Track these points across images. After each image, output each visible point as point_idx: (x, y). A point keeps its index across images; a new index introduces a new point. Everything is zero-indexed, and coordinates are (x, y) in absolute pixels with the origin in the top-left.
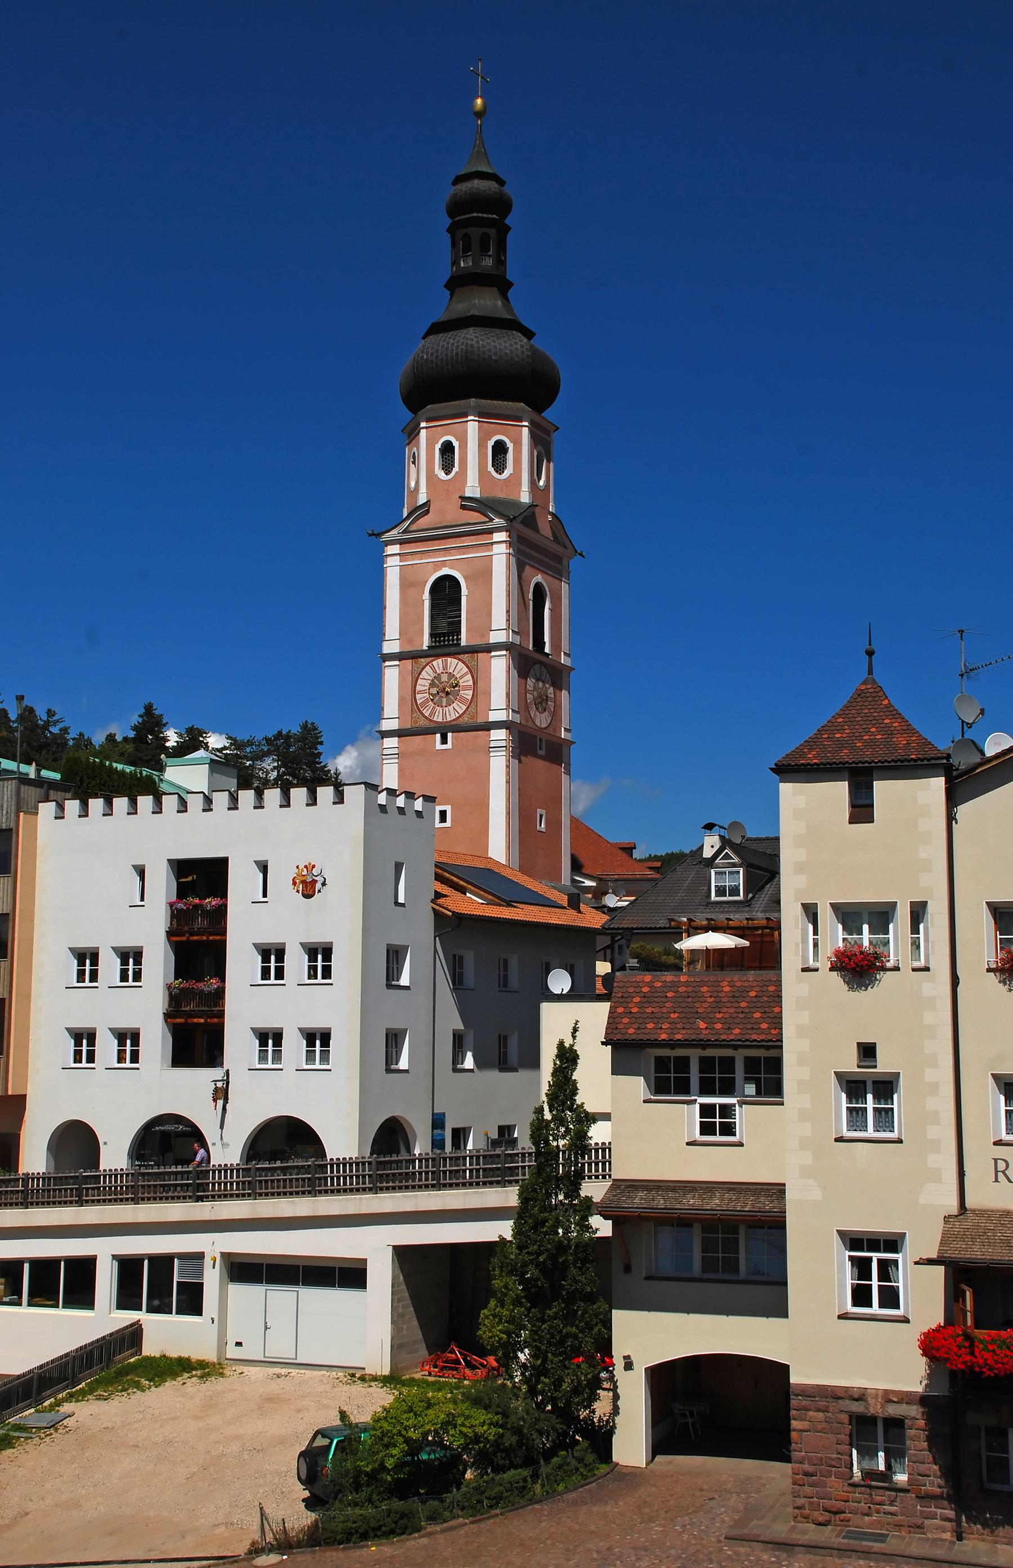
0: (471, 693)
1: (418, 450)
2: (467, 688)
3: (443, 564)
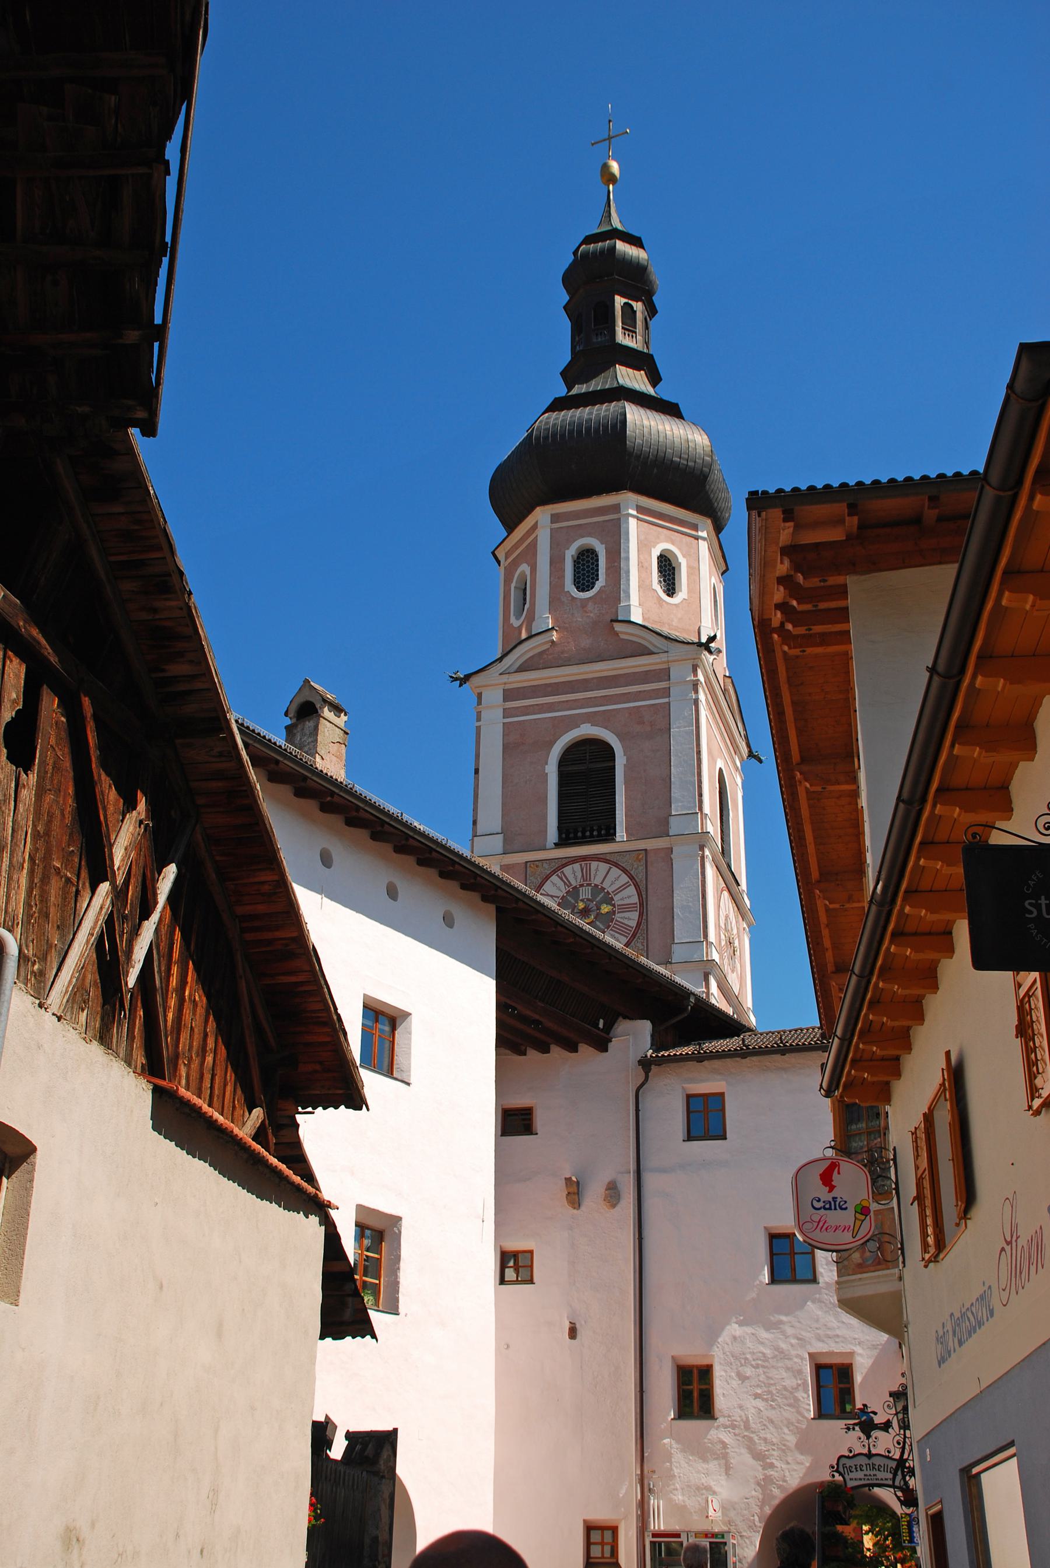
0: (635, 915)
1: (534, 570)
2: (626, 908)
3: (574, 722)
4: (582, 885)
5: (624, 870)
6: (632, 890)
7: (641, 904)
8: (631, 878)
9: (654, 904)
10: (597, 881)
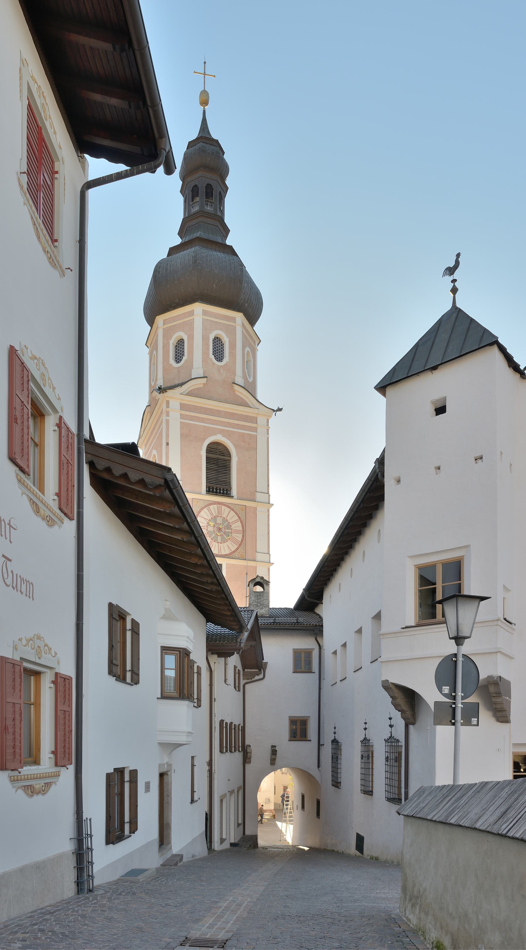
3: (215, 432)
5: (236, 513)
6: (239, 524)
7: (243, 531)
8: (239, 518)
9: (248, 532)
10: (225, 516)
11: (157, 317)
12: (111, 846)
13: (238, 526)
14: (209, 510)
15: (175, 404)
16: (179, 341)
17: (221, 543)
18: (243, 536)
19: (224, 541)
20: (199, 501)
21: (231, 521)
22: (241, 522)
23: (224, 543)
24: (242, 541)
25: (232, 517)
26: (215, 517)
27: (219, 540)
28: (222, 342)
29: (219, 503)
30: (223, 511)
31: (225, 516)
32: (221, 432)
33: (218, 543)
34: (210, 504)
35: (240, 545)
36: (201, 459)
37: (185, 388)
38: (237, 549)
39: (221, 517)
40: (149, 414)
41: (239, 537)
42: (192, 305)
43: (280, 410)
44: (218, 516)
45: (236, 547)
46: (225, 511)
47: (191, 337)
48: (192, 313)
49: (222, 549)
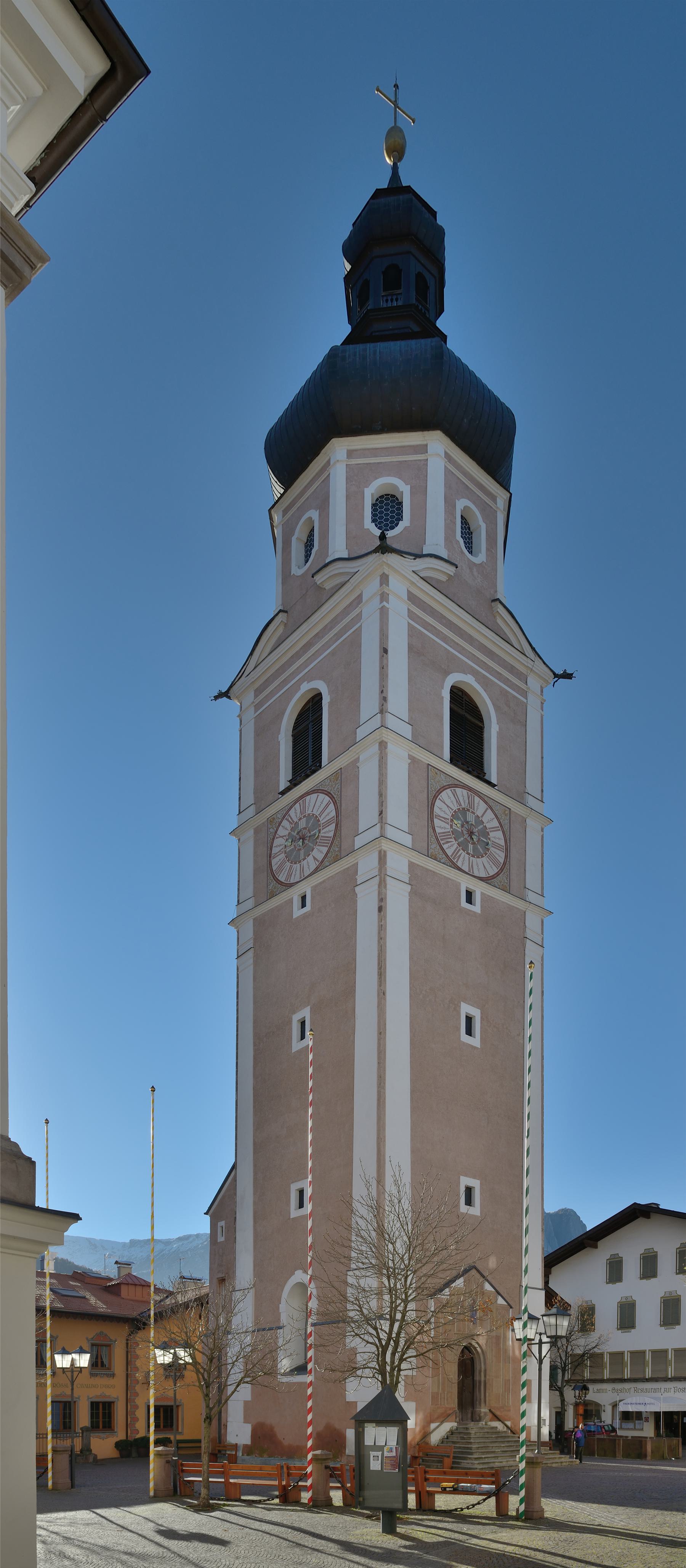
4: (300, 819)
11: (333, 440)
12: (644, 1281)
13: (497, 837)
14: (455, 794)
15: (398, 587)
16: (382, 497)
17: (473, 856)
18: (506, 857)
19: (477, 855)
20: (438, 772)
21: (488, 826)
22: (504, 833)
23: (478, 857)
24: (505, 863)
25: (490, 821)
26: (464, 809)
27: (471, 851)
28: (469, 528)
29: (470, 789)
30: (476, 805)
31: (479, 813)
32: (474, 673)
33: (468, 854)
34: (456, 786)
35: (502, 870)
36: (442, 703)
37: (420, 564)
38: (498, 874)
39: (474, 813)
40: (281, 630)
41: (501, 856)
42: (426, 433)
43: (567, 676)
44: (468, 810)
45: (496, 870)
46: (480, 807)
47: (420, 491)
48: (424, 449)
49: (475, 867)
